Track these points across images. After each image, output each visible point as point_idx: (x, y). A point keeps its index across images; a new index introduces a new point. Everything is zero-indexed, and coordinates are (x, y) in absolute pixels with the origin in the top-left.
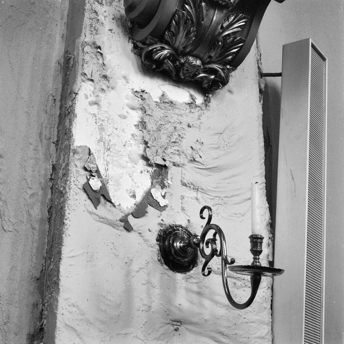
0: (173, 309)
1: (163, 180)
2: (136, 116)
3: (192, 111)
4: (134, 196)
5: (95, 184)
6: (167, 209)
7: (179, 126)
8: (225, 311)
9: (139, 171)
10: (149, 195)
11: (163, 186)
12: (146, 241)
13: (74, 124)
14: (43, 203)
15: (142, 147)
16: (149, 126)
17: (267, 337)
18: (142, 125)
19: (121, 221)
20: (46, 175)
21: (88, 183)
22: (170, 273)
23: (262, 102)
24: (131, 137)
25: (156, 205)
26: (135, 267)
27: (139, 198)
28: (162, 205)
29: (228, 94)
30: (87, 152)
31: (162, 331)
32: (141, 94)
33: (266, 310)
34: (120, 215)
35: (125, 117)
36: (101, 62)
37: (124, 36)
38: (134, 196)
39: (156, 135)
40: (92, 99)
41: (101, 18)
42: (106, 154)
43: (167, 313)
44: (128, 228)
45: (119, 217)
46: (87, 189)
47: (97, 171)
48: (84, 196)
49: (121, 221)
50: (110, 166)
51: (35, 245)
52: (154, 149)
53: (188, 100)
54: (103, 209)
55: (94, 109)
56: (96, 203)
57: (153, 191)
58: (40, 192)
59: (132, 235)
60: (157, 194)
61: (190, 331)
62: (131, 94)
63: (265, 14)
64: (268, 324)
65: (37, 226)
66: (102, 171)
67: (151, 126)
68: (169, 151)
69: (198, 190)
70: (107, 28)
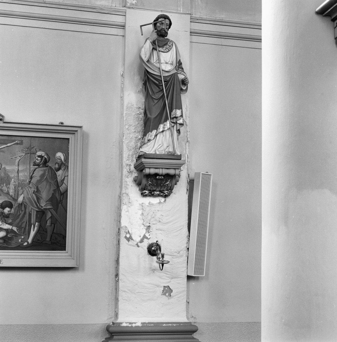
0: (152, 267)
1: (149, 230)
2: (140, 212)
3: (160, 205)
4: (140, 237)
5: (128, 236)
6: (150, 239)
7: (155, 212)
8: (170, 266)
9: (142, 229)
10: (144, 236)
11: (149, 232)
12: (144, 249)
13: (121, 219)
14: (116, 240)
15: (143, 221)
16: (144, 214)
17: (185, 271)
18: (142, 214)
19: (136, 245)
20: (117, 231)
21: (126, 236)
22: (152, 257)
23: (188, 193)
24: (139, 219)
25: (147, 238)
26: (141, 257)
27: (142, 237)
28: (149, 238)
29: (174, 195)
30: (125, 227)
31: (149, 273)
32: (142, 205)
33: (185, 264)
34: (136, 243)
35: (137, 213)
36: (128, 198)
37: (317, 14)
38: (140, 237)
39: (147, 216)
40: (126, 210)
41: (128, 183)
42: (131, 225)
43: (151, 268)
44: (138, 246)
45: (136, 244)
46: (126, 237)
47: (129, 232)
48: (125, 239)
49: (136, 245)
50: (133, 229)
51: (115, 252)
52: (146, 221)
53: (158, 201)
54: (131, 242)
55: (127, 213)
56: (129, 241)
57: (146, 234)
58: (116, 237)
59: (140, 248)
60: (147, 235)
61: (158, 272)
62: (138, 205)
63: (262, 70)
64: (186, 267)
65: (115, 247)
66: (130, 232)
67: (145, 214)
68: (152, 220)
69: (161, 230)
70: (130, 185)
